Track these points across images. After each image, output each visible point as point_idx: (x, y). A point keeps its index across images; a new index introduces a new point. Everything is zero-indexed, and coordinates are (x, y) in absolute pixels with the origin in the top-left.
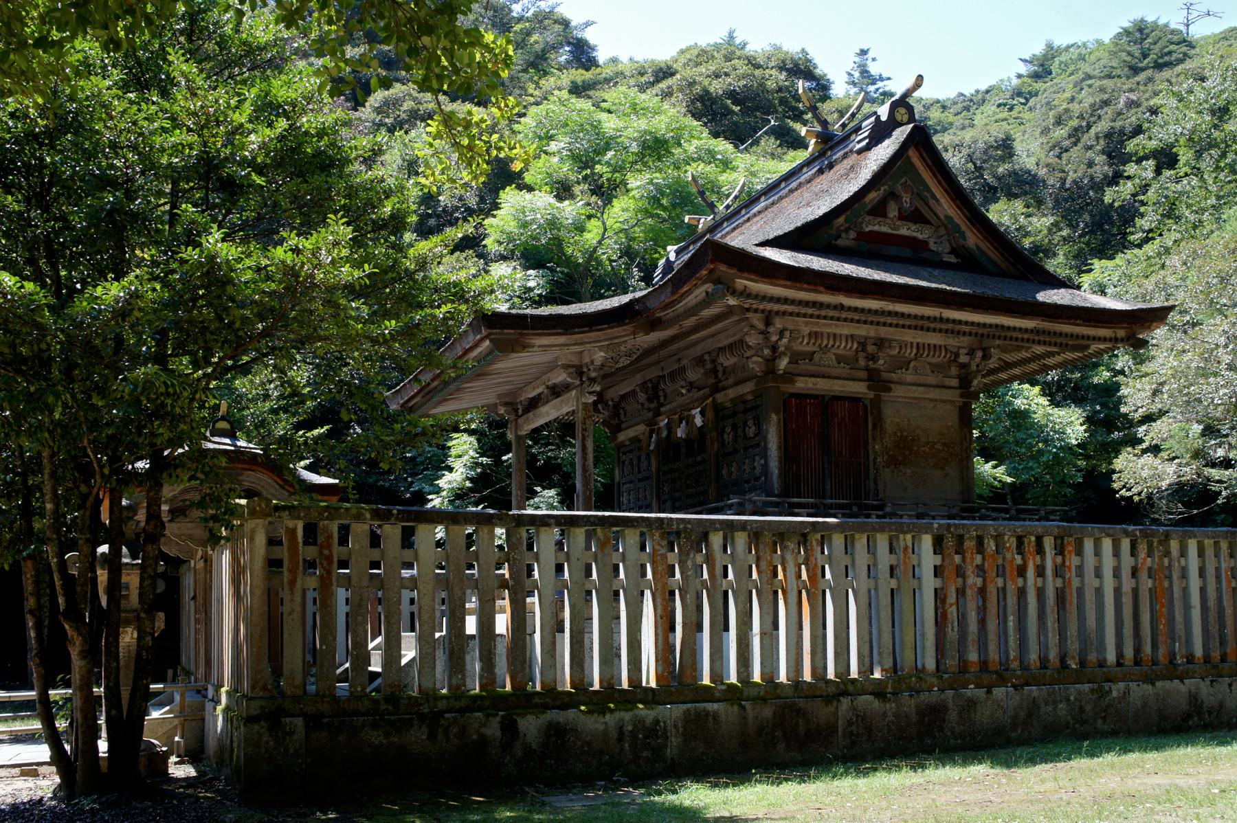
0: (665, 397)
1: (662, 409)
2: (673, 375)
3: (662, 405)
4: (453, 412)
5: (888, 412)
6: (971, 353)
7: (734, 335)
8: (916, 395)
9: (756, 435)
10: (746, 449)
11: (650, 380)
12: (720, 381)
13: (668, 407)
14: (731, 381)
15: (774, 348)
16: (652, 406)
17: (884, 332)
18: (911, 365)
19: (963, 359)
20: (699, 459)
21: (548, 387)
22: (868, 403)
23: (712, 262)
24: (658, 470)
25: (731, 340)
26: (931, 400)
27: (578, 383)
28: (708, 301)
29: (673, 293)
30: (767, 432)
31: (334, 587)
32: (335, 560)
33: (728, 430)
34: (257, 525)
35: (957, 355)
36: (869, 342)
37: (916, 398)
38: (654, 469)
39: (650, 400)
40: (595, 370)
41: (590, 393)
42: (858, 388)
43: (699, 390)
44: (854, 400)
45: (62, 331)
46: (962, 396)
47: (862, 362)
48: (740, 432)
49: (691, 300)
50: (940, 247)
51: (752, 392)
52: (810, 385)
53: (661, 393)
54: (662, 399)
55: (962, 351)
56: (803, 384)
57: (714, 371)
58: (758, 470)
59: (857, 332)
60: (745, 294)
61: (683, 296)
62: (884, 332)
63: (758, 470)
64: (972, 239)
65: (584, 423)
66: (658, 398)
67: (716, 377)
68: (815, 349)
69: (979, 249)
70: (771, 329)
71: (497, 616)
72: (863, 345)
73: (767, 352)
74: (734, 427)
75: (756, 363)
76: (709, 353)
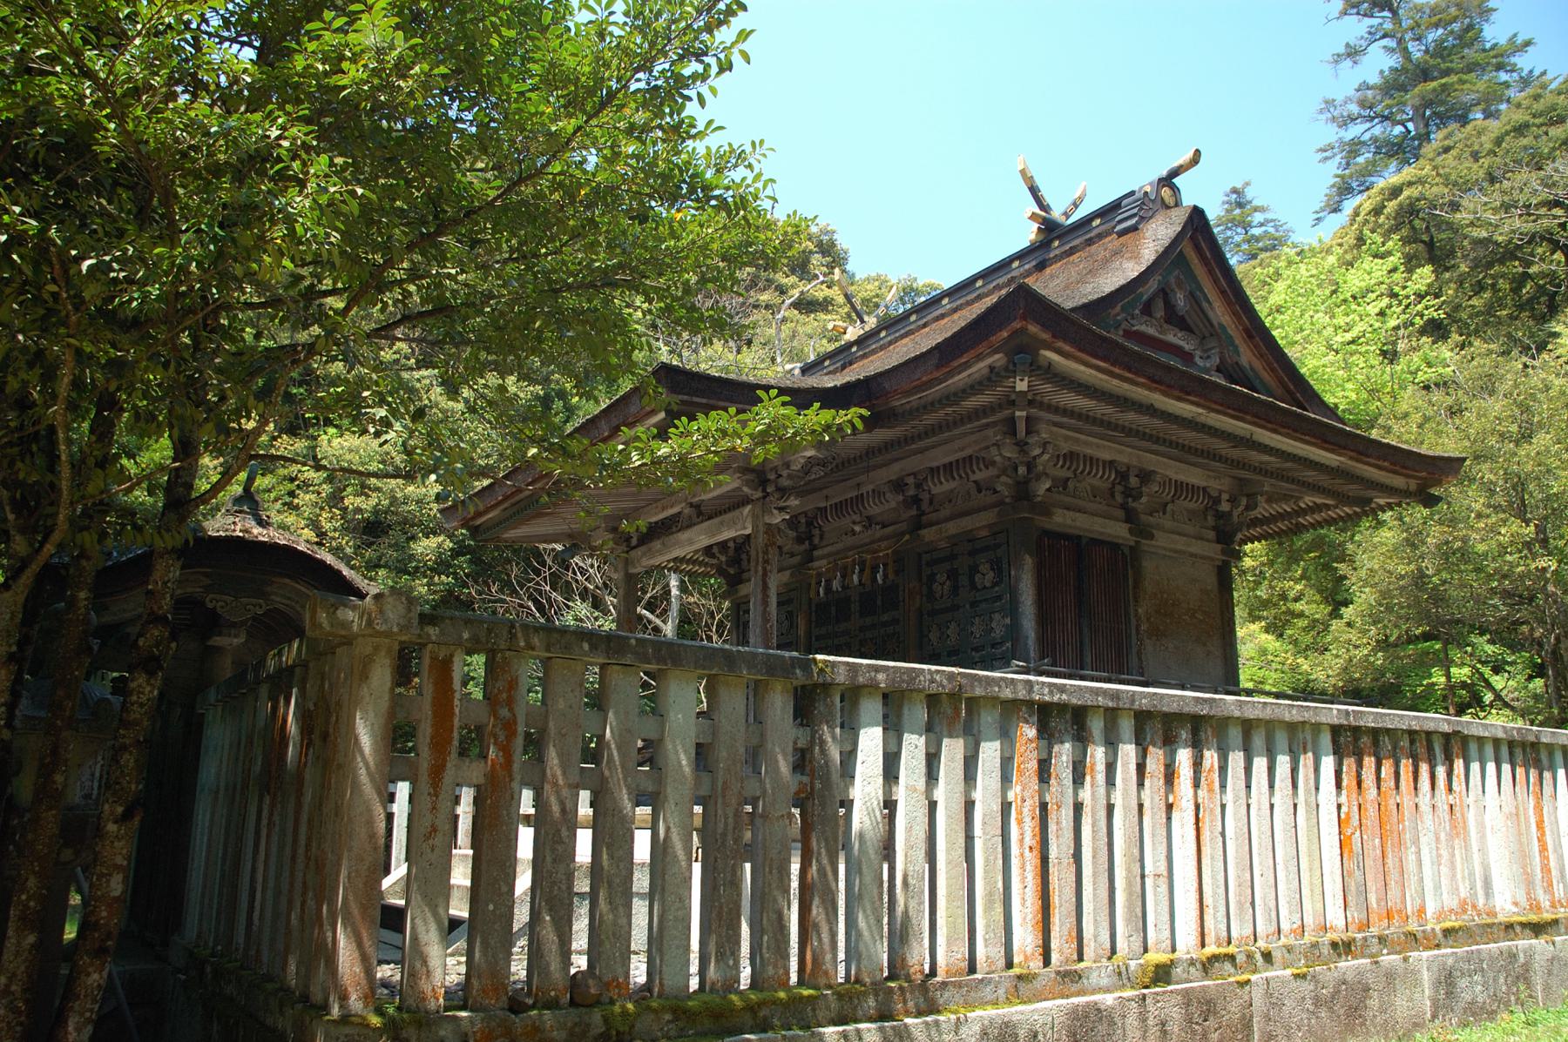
0: (822, 537)
1: (816, 553)
2: (840, 508)
3: (815, 548)
4: (530, 538)
5: (1148, 565)
6: (1233, 500)
7: (962, 449)
8: (1179, 547)
9: (995, 584)
10: (974, 604)
11: (805, 513)
12: (923, 513)
13: (826, 551)
14: (945, 512)
15: (1030, 466)
16: (802, 548)
17: (1151, 461)
18: (1169, 507)
19: (1225, 507)
20: (885, 617)
21: (691, 505)
22: (1127, 551)
23: (1024, 318)
24: (809, 633)
25: (947, 460)
26: (1192, 555)
27: (759, 494)
28: (994, 377)
29: (938, 367)
30: (1018, 579)
31: (515, 785)
32: (521, 729)
33: (941, 578)
34: (376, 649)
35: (1217, 501)
36: (1132, 473)
37: (1176, 551)
38: (801, 632)
39: (799, 540)
40: (790, 477)
41: (781, 509)
42: (1118, 531)
43: (884, 526)
44: (1114, 547)
45: (37, 184)
46: (1223, 552)
47: (1119, 498)
48: (964, 580)
49: (960, 379)
50: (1206, 366)
51: (989, 526)
52: (1069, 522)
53: (816, 532)
54: (816, 541)
55: (1225, 496)
56: (1062, 520)
57: (916, 500)
58: (998, 632)
59: (1119, 458)
60: (1050, 374)
61: (951, 374)
62: (1151, 461)
63: (998, 632)
64: (1246, 356)
65: (766, 553)
66: (810, 537)
67: (919, 508)
68: (1070, 474)
69: (1252, 369)
70: (1033, 440)
71: (579, 831)
72: (1123, 476)
73: (1022, 470)
74: (953, 575)
75: (1005, 484)
76: (914, 474)
